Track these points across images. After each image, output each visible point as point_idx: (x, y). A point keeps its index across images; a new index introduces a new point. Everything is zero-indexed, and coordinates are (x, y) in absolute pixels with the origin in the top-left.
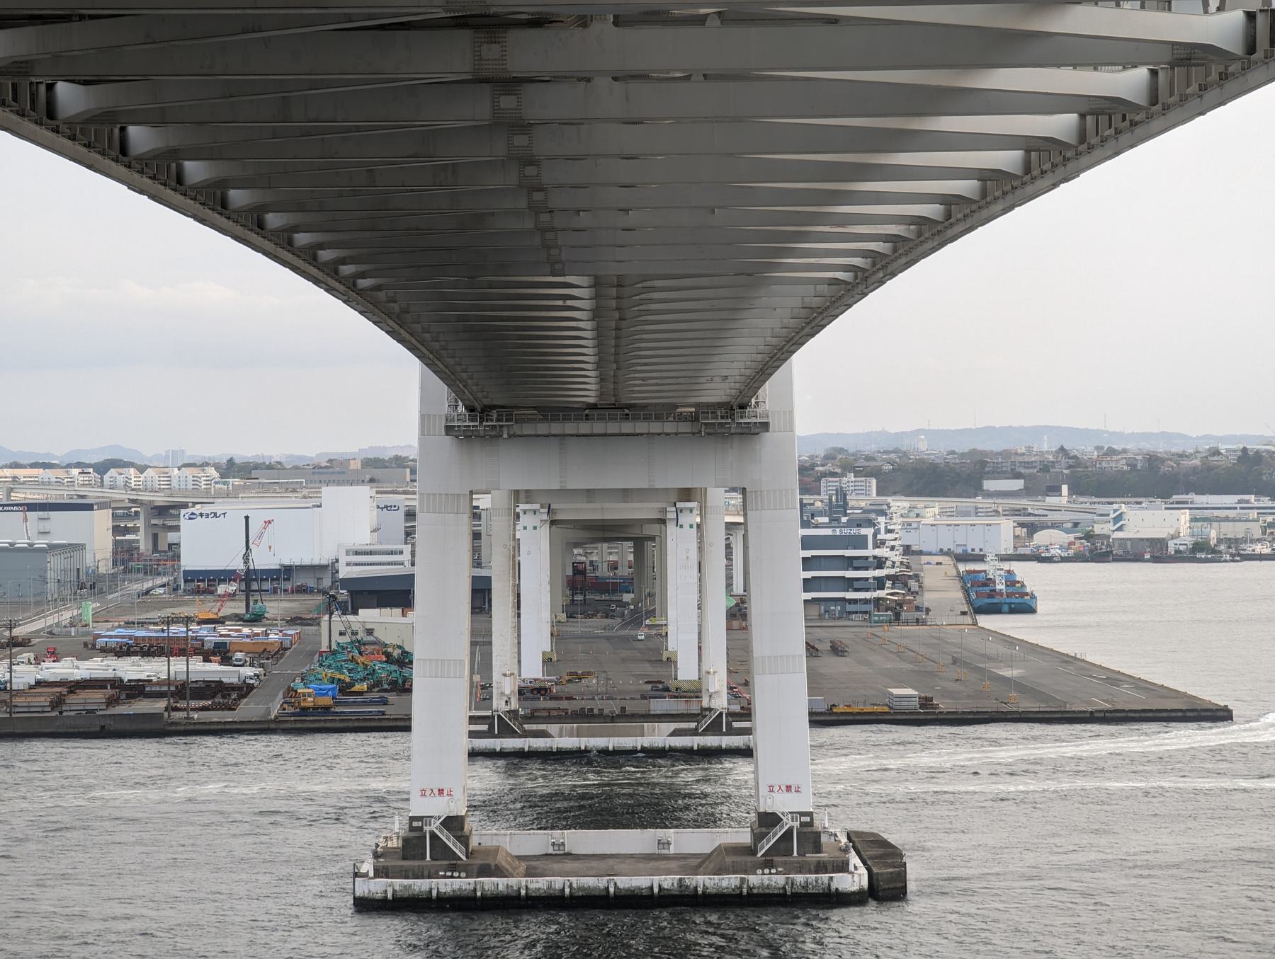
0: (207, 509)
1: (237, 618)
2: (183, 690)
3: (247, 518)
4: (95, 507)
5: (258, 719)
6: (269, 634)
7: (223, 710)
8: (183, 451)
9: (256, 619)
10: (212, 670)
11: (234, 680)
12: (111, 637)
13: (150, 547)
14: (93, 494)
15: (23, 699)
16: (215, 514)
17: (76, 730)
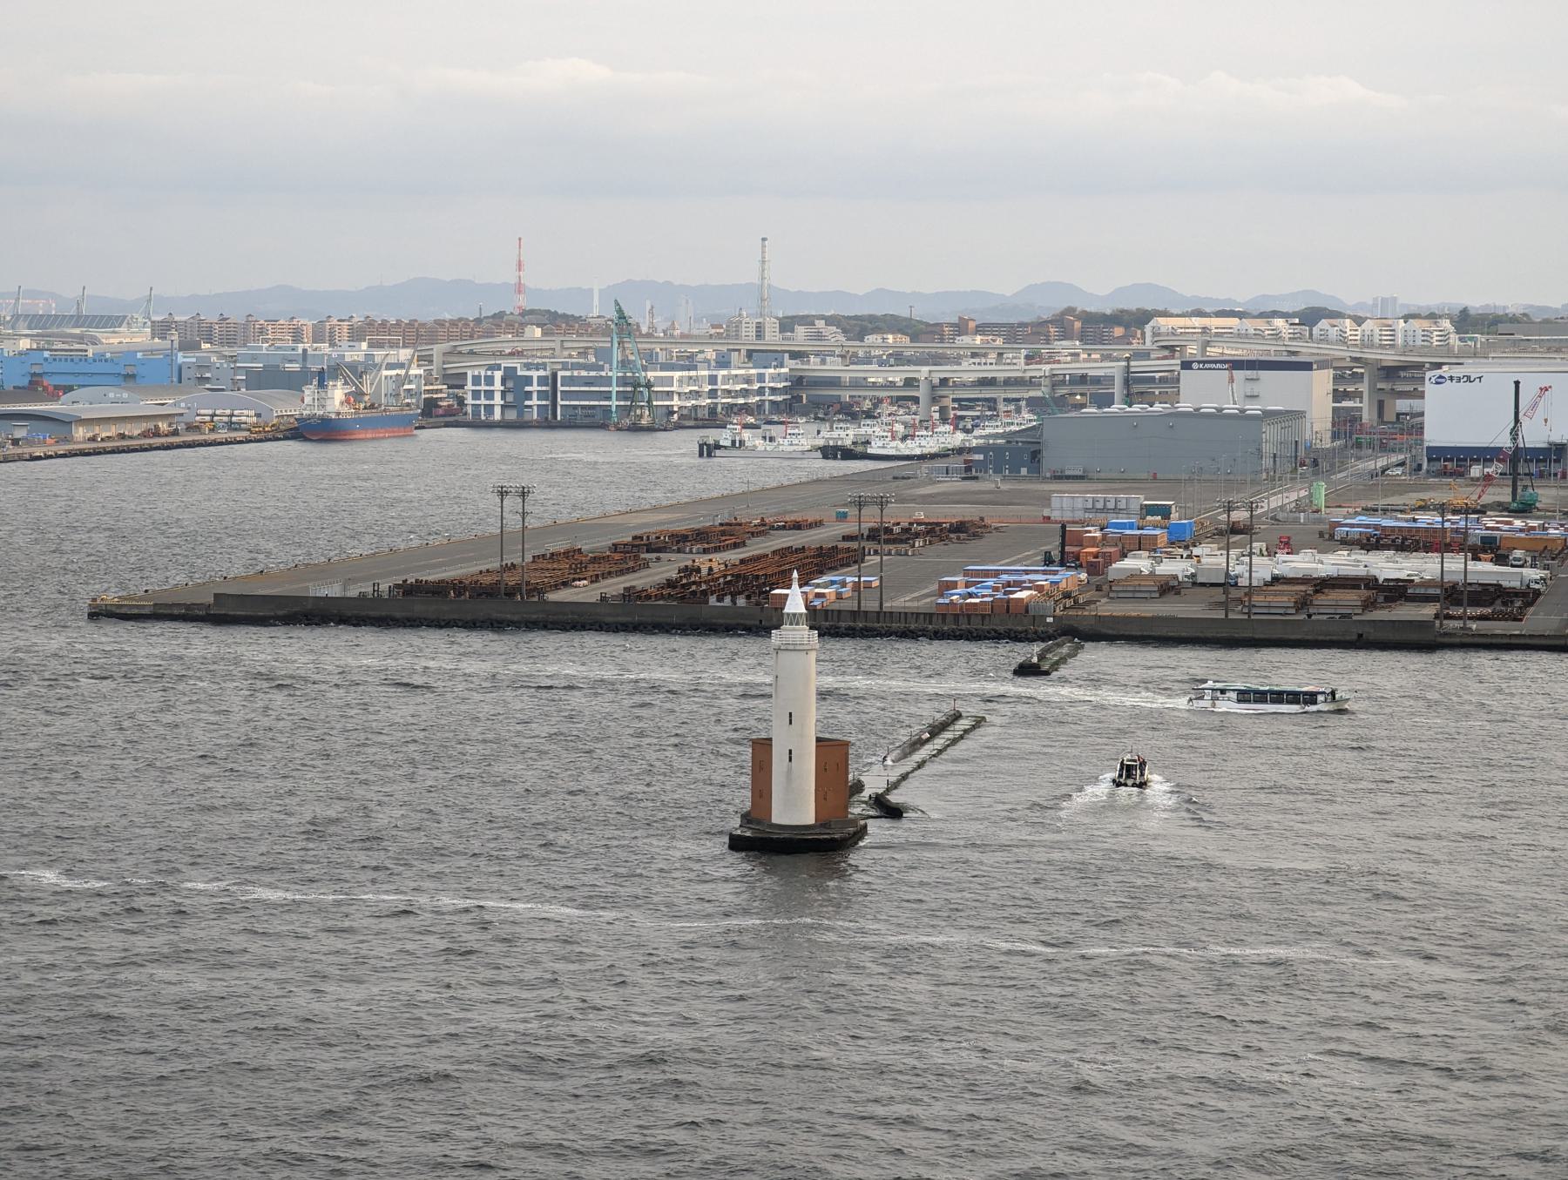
0: (1457, 371)
1: (1501, 507)
2: (1452, 594)
3: (1517, 383)
4: (1315, 366)
5: (1552, 633)
6: (1547, 529)
7: (1506, 620)
8: (1395, 299)
9: (1525, 510)
10: (1485, 570)
11: (1517, 584)
12: (1352, 526)
13: (1375, 416)
14: (1306, 351)
15: (1261, 598)
16: (1469, 377)
17: (1328, 638)
